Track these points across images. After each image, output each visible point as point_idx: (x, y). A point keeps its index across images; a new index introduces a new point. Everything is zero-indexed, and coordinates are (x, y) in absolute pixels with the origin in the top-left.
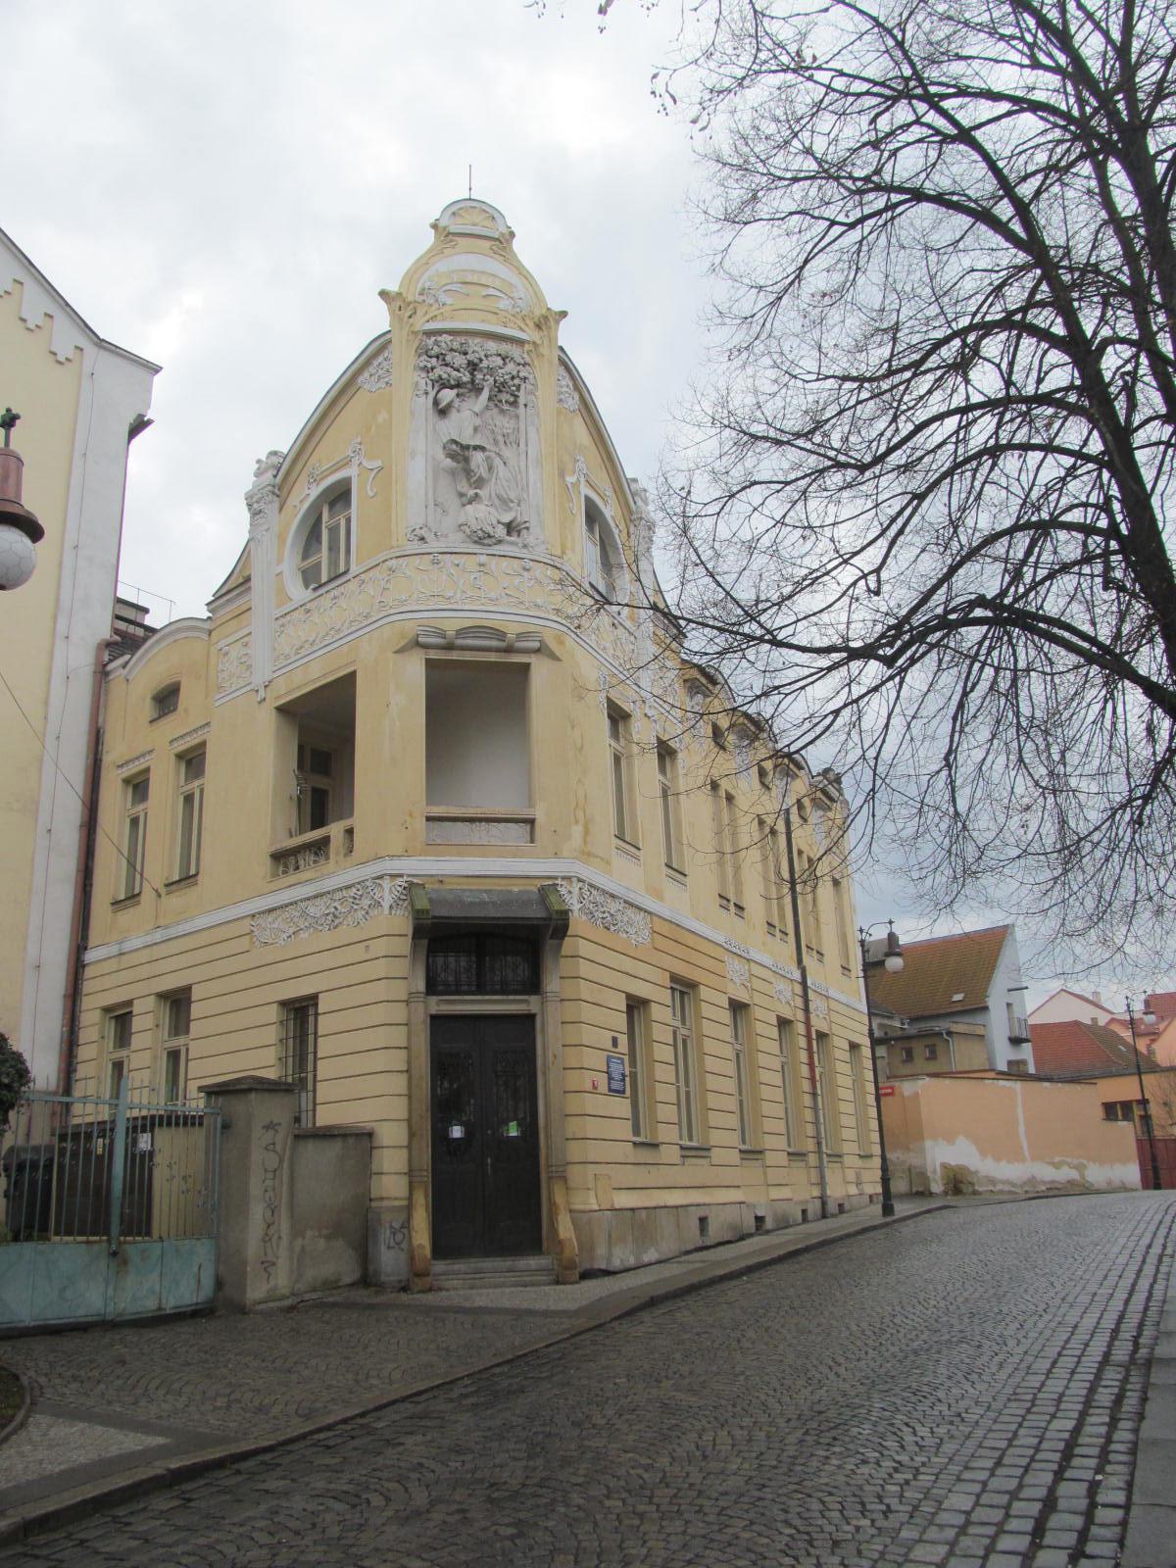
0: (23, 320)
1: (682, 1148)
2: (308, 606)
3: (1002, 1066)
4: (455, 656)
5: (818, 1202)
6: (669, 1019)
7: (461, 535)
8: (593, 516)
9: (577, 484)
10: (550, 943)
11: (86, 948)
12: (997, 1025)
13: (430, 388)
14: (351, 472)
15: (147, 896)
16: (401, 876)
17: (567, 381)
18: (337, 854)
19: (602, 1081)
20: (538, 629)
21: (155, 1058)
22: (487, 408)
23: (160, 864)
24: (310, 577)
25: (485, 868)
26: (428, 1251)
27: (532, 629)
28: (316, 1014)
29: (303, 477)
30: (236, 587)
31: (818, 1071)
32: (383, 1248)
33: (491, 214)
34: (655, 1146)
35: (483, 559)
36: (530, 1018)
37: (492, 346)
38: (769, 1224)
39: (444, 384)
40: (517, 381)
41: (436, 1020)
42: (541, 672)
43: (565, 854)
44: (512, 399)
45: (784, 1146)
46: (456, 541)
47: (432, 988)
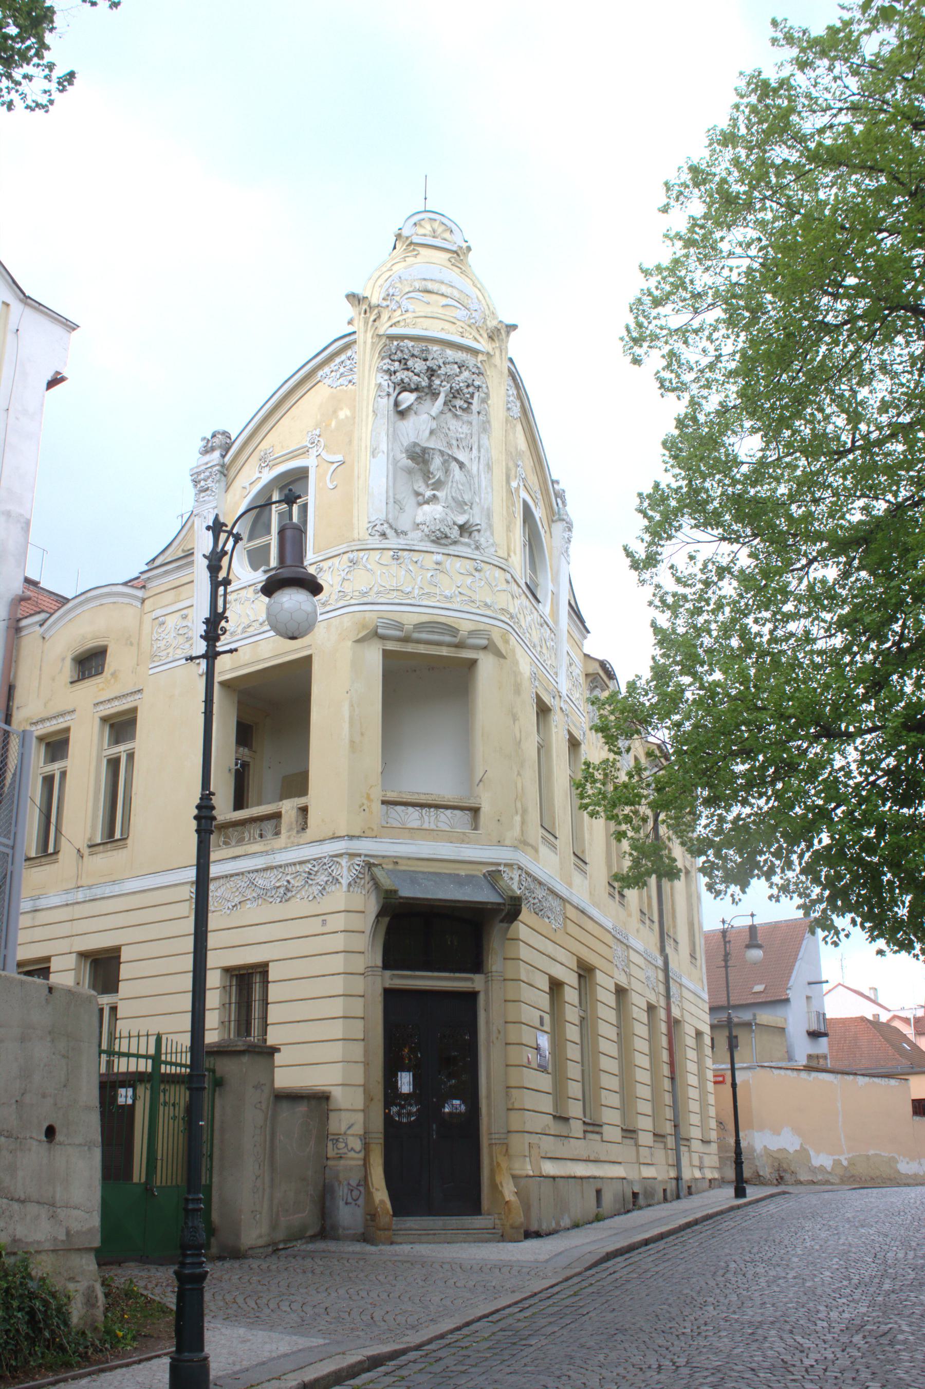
1: (584, 1123)
3: (802, 1061)
4: (410, 648)
9: (517, 489)
12: (796, 1020)
13: (391, 390)
17: (513, 391)
18: (290, 830)
20: (488, 627)
22: (442, 413)
25: (438, 855)
27: (482, 627)
32: (341, 1203)
34: (566, 1119)
35: (439, 558)
36: (472, 996)
37: (450, 354)
39: (404, 387)
40: (471, 389)
41: (389, 994)
42: (486, 665)
43: (508, 842)
46: (414, 538)
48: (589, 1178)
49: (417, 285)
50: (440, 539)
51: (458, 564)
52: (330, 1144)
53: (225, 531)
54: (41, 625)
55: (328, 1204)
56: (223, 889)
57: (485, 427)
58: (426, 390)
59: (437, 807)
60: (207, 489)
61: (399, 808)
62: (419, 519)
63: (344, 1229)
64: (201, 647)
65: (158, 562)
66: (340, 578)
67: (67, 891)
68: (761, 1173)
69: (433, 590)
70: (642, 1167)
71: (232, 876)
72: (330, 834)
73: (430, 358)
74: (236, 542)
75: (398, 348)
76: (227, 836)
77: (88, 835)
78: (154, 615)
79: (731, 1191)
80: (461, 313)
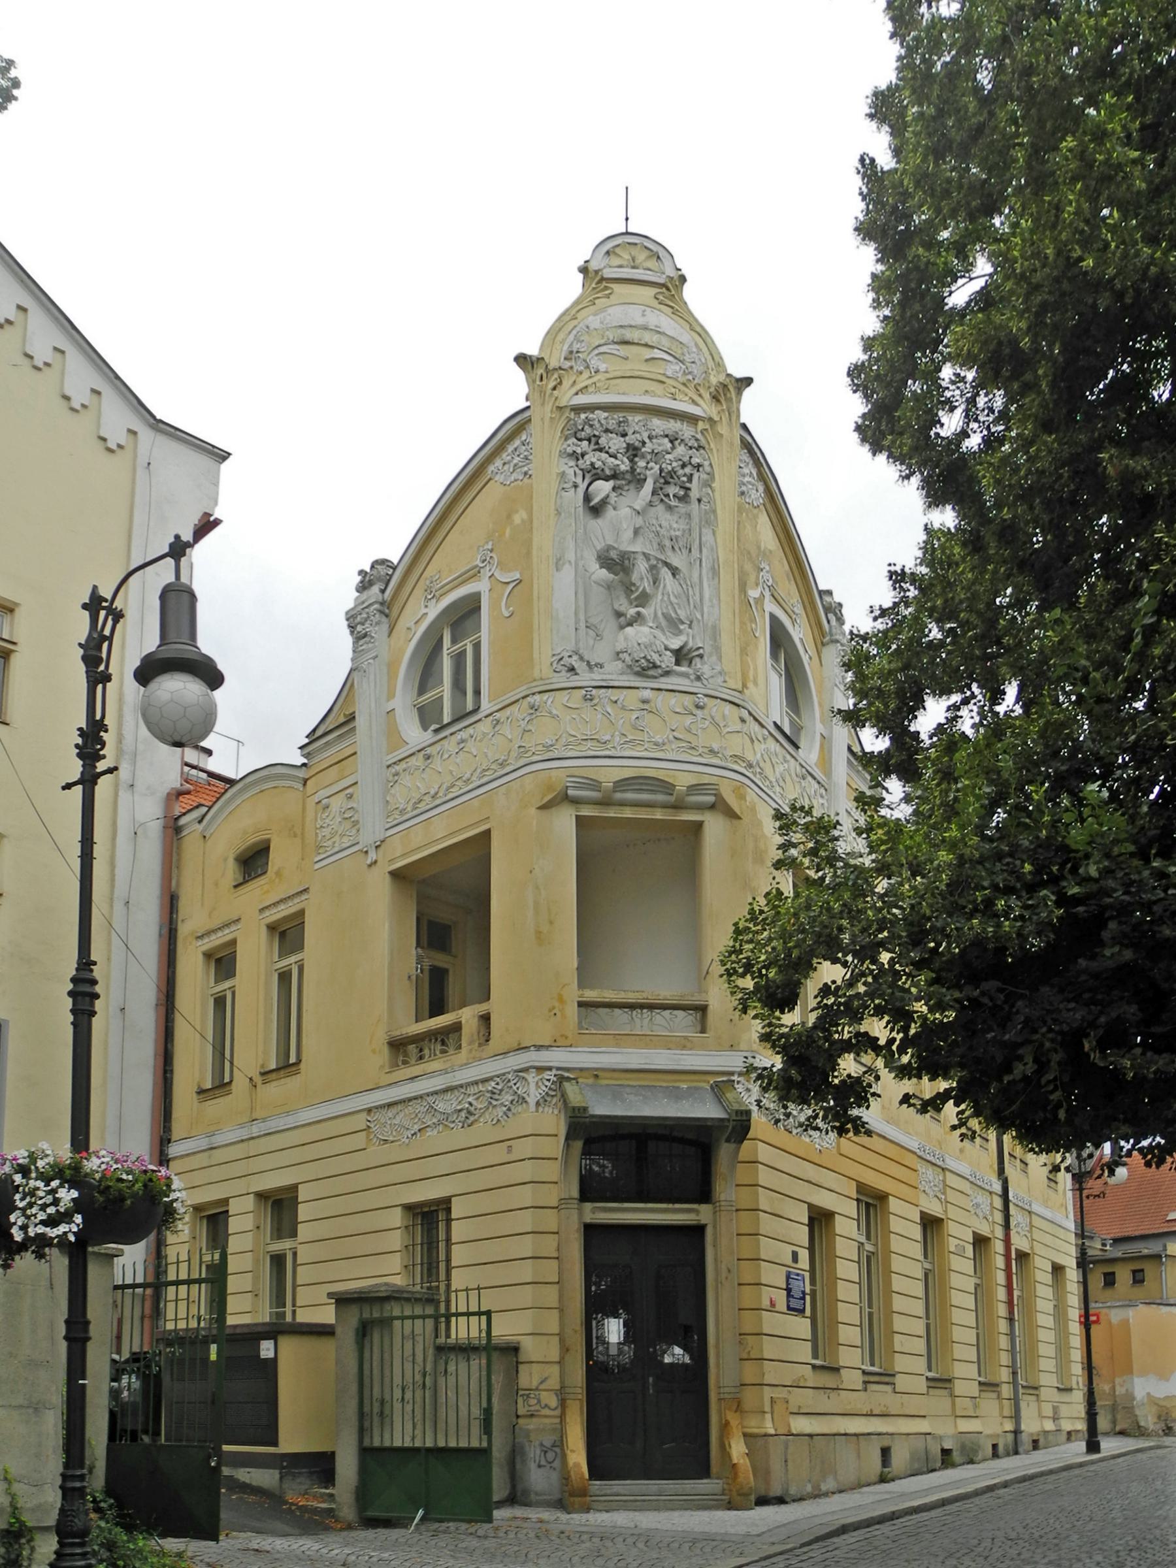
0: (67, 398)
1: (864, 1372)
2: (429, 751)
4: (611, 813)
5: (1010, 1437)
6: (854, 1234)
7: (619, 664)
8: (779, 640)
9: (760, 600)
10: (724, 1151)
11: (169, 1141)
13: (579, 480)
14: (481, 586)
15: (240, 1084)
16: (550, 1069)
18: (471, 1043)
19: (781, 1298)
20: (714, 780)
21: (256, 1261)
22: (650, 504)
23: (253, 1046)
24: (427, 715)
26: (587, 1476)
28: (449, 1221)
29: (419, 591)
30: (335, 727)
31: (1016, 1293)
33: (656, 252)
34: (836, 1370)
35: (647, 694)
36: (698, 1231)
38: (956, 1456)
39: (596, 474)
40: (688, 470)
41: (591, 1231)
42: (714, 827)
44: (682, 493)
45: (976, 1376)
46: (613, 672)
47: (590, 1190)
48: (869, 1434)
49: (610, 335)
50: (646, 669)
51: (673, 700)
52: (520, 1400)
53: (104, 608)
54: (200, 822)
55: (518, 1466)
56: (402, 1115)
57: (710, 519)
58: (628, 476)
59: (651, 1007)
60: (365, 635)
61: (601, 1011)
62: (620, 646)
63: (536, 1494)
64: (75, 769)
65: (319, 733)
66: (520, 730)
67: (241, 1126)
68: (1142, 1424)
69: (639, 736)
70: (959, 1421)
71: (410, 1100)
72: (515, 1046)
73: (630, 432)
74: (116, 622)
75: (587, 422)
76: (406, 1054)
77: (260, 1062)
78: (316, 798)
79: (1082, 1446)
80: (673, 368)
